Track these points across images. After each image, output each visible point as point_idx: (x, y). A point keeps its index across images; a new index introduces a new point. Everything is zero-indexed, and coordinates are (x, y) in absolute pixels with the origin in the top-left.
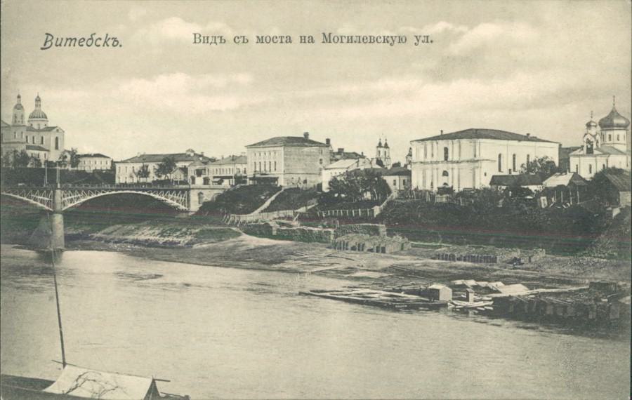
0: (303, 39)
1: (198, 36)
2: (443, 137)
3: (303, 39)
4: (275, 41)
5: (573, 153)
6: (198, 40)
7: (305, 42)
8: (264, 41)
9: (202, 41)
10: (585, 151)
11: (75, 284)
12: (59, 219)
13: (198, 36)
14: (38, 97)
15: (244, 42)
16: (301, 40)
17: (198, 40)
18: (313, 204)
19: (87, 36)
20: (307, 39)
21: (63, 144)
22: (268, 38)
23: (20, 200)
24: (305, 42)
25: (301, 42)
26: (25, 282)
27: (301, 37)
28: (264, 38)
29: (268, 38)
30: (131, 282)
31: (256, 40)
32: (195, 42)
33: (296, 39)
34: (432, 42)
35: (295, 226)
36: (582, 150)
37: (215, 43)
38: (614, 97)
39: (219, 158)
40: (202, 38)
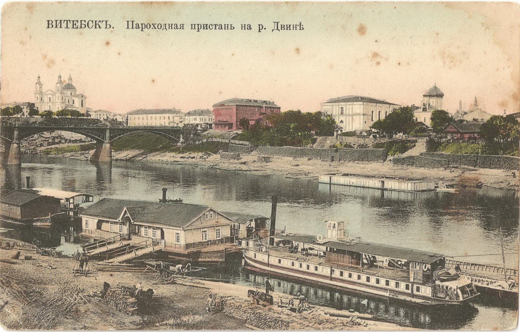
0: (243, 27)
1: (50, 22)
3: (243, 27)
8: (208, 28)
9: (54, 26)
10: (422, 110)
12: (108, 131)
15: (300, 29)
16: (183, 27)
17: (50, 26)
19: (202, 30)
22: (148, 27)
23: (82, 118)
24: (287, 25)
26: (4, 230)
27: (48, 21)
28: (208, 26)
29: (148, 27)
30: (216, 165)
34: (265, 29)
36: (367, 281)
37: (277, 29)
38: (342, 113)
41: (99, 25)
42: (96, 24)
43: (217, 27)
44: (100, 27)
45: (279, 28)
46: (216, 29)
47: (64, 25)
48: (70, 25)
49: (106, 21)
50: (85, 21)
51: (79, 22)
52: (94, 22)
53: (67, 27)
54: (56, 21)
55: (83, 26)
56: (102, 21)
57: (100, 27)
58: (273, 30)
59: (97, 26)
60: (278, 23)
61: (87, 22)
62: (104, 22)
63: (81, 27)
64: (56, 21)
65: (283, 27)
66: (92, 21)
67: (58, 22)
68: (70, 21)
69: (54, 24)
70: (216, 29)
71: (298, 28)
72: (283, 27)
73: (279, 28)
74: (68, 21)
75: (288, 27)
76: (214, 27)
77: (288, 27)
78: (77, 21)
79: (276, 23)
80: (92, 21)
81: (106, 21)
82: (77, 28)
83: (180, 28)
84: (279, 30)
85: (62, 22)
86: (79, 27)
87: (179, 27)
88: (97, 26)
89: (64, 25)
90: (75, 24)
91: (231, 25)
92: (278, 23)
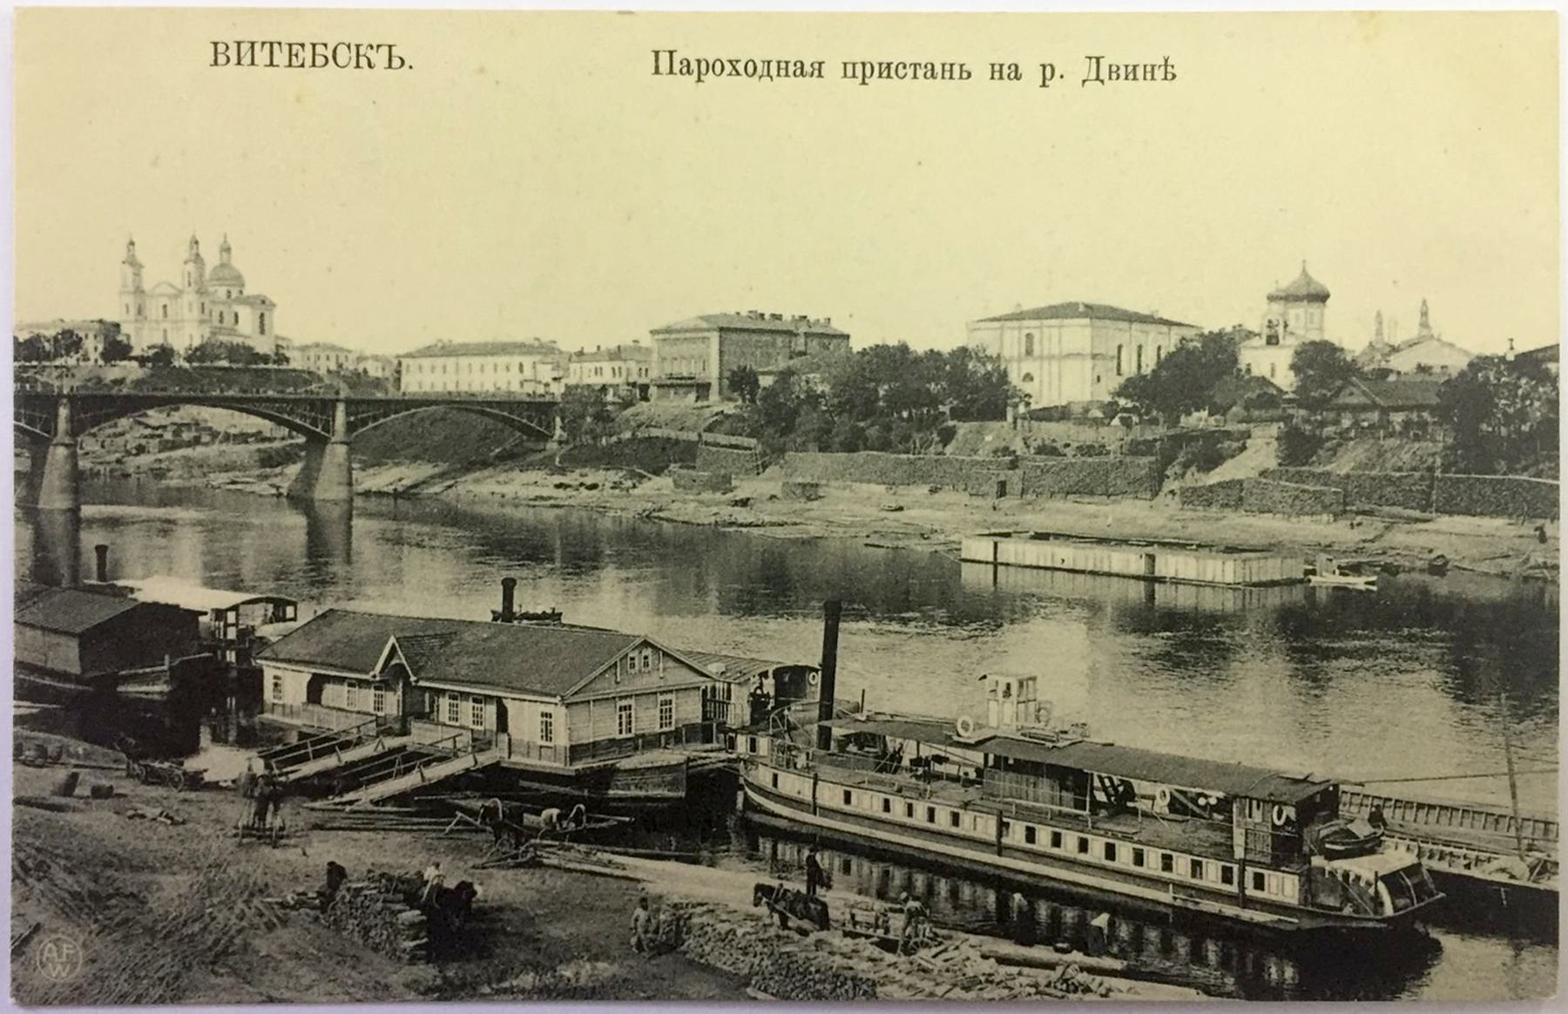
0: (997, 71)
1: (221, 48)
2: (1019, 316)
3: (997, 71)
4: (901, 72)
5: (1247, 343)
7: (787, 75)
9: (234, 59)
10: (1264, 341)
11: (1517, 541)
12: (341, 408)
14: (194, 237)
16: (993, 72)
17: (222, 59)
18: (973, 410)
20: (791, 68)
21: (272, 327)
25: (992, 78)
28: (893, 67)
31: (1084, 69)
32: (390, 67)
33: (981, 72)
35: (643, 413)
39: (590, 349)
41: (369, 60)
42: (358, 55)
43: (920, 73)
44: (370, 65)
45: (1104, 74)
46: (915, 77)
47: (262, 56)
48: (281, 57)
49: (390, 47)
50: (325, 45)
51: (309, 48)
52: (353, 49)
53: (271, 64)
54: (239, 43)
55: (320, 61)
56: (379, 46)
57: (370, 65)
58: (1084, 81)
59: (363, 62)
60: (1098, 59)
61: (331, 48)
62: (385, 50)
63: (314, 65)
64: (239, 43)
65: (1114, 72)
66: (349, 47)
67: (245, 47)
68: (280, 43)
69: (233, 53)
70: (915, 77)
71: (1159, 74)
72: (1114, 72)
73: (1104, 74)
74: (276, 46)
75: (1132, 73)
76: (910, 71)
77: (1132, 73)
78: (302, 45)
79: (1094, 60)
80: (349, 47)
81: (390, 47)
82: (302, 66)
83: (812, 74)
84: (1102, 81)
85: (257, 47)
86: (309, 62)
87: (808, 69)
88: (363, 62)
89: (262, 56)
90: (296, 55)
91: (961, 66)
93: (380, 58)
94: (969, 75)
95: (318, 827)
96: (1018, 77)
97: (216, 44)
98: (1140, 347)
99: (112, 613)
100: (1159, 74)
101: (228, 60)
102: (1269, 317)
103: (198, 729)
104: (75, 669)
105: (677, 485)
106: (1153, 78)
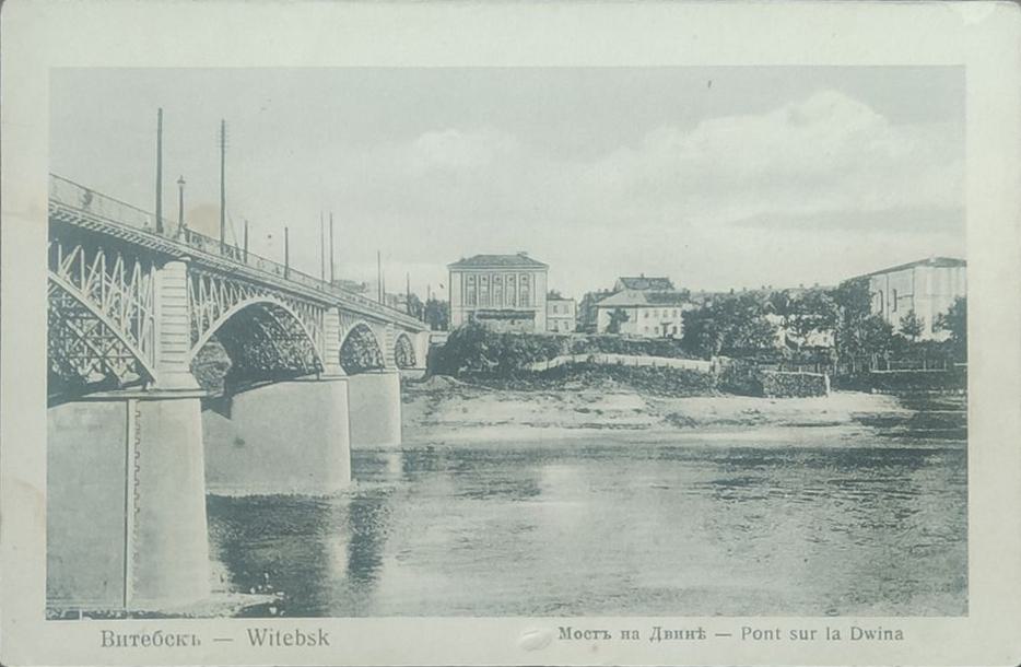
1: (108, 635)
4: (588, 636)
6: (108, 642)
9: (116, 643)
13: (108, 635)
17: (108, 642)
40: (115, 639)
43: (138, 641)
45: (663, 635)
47: (130, 642)
60: (659, 628)
73: (663, 635)
89: (130, 642)
92: (659, 628)
93: (188, 641)
94: (199, 643)
95: (383, 451)
96: (838, 638)
97: (104, 632)
98: (160, 110)
99: (146, 365)
100: (696, 635)
101: (113, 642)
102: (733, 287)
103: (91, 384)
104: (198, 387)
105: (728, 471)
106: (125, 645)
